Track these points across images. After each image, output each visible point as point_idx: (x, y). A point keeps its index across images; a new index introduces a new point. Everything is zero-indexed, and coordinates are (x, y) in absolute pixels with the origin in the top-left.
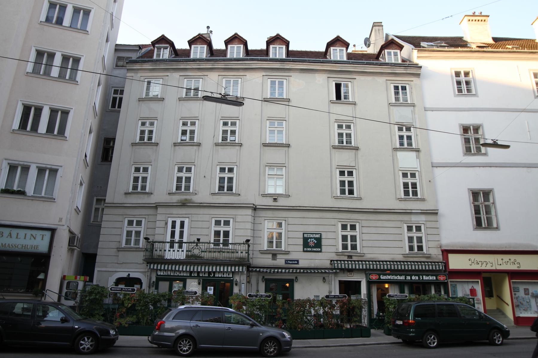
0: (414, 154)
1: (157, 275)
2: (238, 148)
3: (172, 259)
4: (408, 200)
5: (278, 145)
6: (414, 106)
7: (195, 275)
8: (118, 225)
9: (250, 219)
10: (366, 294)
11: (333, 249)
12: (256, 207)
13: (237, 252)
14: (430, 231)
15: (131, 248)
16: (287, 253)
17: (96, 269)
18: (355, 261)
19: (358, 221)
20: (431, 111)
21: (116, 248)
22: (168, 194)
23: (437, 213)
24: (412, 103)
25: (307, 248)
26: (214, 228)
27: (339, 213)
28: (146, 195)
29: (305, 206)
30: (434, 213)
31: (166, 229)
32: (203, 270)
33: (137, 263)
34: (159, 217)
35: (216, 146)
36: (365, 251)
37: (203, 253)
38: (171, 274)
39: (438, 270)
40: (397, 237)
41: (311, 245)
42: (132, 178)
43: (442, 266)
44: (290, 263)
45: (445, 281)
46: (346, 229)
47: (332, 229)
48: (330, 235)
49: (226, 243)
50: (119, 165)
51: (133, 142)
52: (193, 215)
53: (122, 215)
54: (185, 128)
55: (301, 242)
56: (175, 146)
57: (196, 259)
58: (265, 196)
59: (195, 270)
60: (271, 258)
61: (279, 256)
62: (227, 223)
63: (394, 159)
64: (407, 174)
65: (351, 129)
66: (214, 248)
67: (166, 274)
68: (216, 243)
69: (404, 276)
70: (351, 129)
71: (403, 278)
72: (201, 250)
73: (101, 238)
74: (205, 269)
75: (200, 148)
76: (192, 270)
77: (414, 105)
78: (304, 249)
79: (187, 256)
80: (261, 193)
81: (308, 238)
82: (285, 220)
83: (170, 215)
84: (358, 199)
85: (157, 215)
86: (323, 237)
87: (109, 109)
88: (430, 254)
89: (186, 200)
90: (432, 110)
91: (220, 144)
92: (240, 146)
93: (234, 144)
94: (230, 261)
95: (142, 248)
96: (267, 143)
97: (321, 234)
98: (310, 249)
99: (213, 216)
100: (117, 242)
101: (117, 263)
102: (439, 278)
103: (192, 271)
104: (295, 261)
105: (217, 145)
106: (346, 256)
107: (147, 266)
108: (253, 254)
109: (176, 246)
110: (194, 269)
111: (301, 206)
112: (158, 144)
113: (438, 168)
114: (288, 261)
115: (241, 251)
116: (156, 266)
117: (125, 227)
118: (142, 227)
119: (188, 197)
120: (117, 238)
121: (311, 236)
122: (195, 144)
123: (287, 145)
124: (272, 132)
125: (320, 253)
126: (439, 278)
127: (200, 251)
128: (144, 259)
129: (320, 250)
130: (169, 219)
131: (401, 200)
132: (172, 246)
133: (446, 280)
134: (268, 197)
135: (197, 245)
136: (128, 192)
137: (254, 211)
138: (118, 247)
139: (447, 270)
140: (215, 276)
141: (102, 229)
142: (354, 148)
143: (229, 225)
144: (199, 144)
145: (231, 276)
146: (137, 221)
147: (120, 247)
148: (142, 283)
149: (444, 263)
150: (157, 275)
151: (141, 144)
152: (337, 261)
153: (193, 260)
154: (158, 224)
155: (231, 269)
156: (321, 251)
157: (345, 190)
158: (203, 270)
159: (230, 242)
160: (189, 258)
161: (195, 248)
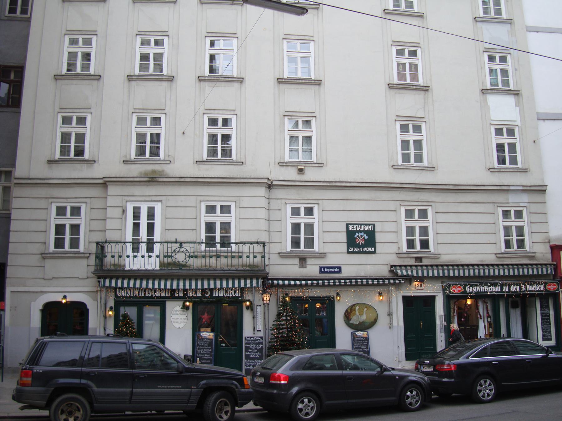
0: (510, 100)
1: (116, 296)
2: (237, 85)
3: (141, 270)
4: (503, 170)
5: (303, 81)
6: (510, 23)
7: (180, 295)
8: (41, 215)
9: (263, 202)
10: (444, 315)
11: (394, 249)
12: (272, 182)
13: (241, 257)
14: (535, 218)
15: (76, 254)
16: (322, 255)
17: (9, 290)
18: (426, 266)
19: (430, 203)
20: (536, 33)
21: (39, 253)
22: (122, 162)
23: (545, 190)
24: (508, 18)
25: (353, 247)
26: (205, 218)
27: (402, 192)
28: (86, 165)
29: (348, 181)
30: (541, 190)
31: (124, 220)
32: (193, 287)
33: (78, 278)
34: (111, 201)
35: (280, 83)
36: (441, 250)
37: (192, 259)
38: (140, 295)
39: (545, 274)
40: (490, 228)
41: (359, 242)
42: (59, 136)
43: (551, 269)
44: (327, 272)
45: (556, 291)
46: (299, 214)
47: (391, 216)
48: (390, 227)
49: (225, 242)
50: (34, 112)
51: (56, 74)
52: (169, 197)
53: (46, 198)
54: (145, 50)
55: (343, 238)
56: (130, 80)
57: (181, 269)
58: (285, 164)
59: (181, 287)
60: (298, 263)
61: (309, 261)
62: (225, 209)
63: (484, 107)
64: (502, 130)
65: (417, 57)
66: (205, 251)
67: (132, 295)
68: (210, 241)
69: (500, 287)
70: (417, 57)
71: (495, 289)
72: (188, 254)
73: (13, 237)
74: (166, 285)
75: (174, 84)
76: (175, 287)
77: (510, 21)
78: (348, 249)
79: (162, 264)
80: (278, 161)
81: (354, 232)
82: (318, 204)
83: (130, 197)
84: (429, 169)
85: (106, 198)
86: (377, 229)
87: (6, 15)
88: (535, 253)
89: (154, 172)
90: (538, 30)
91: (207, 78)
92: (241, 82)
93: (230, 79)
94: (237, 270)
95: (84, 253)
96: (285, 77)
97: (374, 225)
98: (359, 249)
99: (202, 198)
100: (40, 244)
101: (44, 279)
102: (548, 287)
103: (175, 289)
104: (335, 268)
105: (201, 79)
106: (412, 259)
107: (99, 282)
108: (269, 258)
109: (143, 247)
110: (178, 285)
111: (342, 181)
112: (100, 76)
113: (546, 121)
114: (324, 268)
115: (255, 254)
116: (150, 282)
117: (52, 219)
118: (81, 219)
119: (157, 167)
120: (40, 237)
121: (360, 228)
122: (164, 77)
123: (317, 82)
124: (292, 59)
125: (373, 255)
126: (548, 287)
127: (187, 257)
128: (94, 271)
129: (373, 249)
130: (129, 204)
131: (491, 170)
132: (136, 249)
133: (558, 289)
134: (289, 167)
135: (181, 246)
136: (54, 160)
137: (268, 190)
138: (43, 252)
139: (559, 275)
140: (213, 294)
141: (12, 221)
142: (423, 88)
143: (229, 213)
144: (172, 78)
145: (238, 294)
146: (73, 208)
147: (46, 252)
148: (88, 310)
149: (554, 265)
150: (116, 296)
151: (71, 77)
152: (400, 266)
153: (175, 271)
154: (110, 212)
155: (240, 283)
156: (374, 252)
157: (504, 157)
158: (193, 287)
159: (233, 240)
160: (164, 268)
161: (179, 252)
